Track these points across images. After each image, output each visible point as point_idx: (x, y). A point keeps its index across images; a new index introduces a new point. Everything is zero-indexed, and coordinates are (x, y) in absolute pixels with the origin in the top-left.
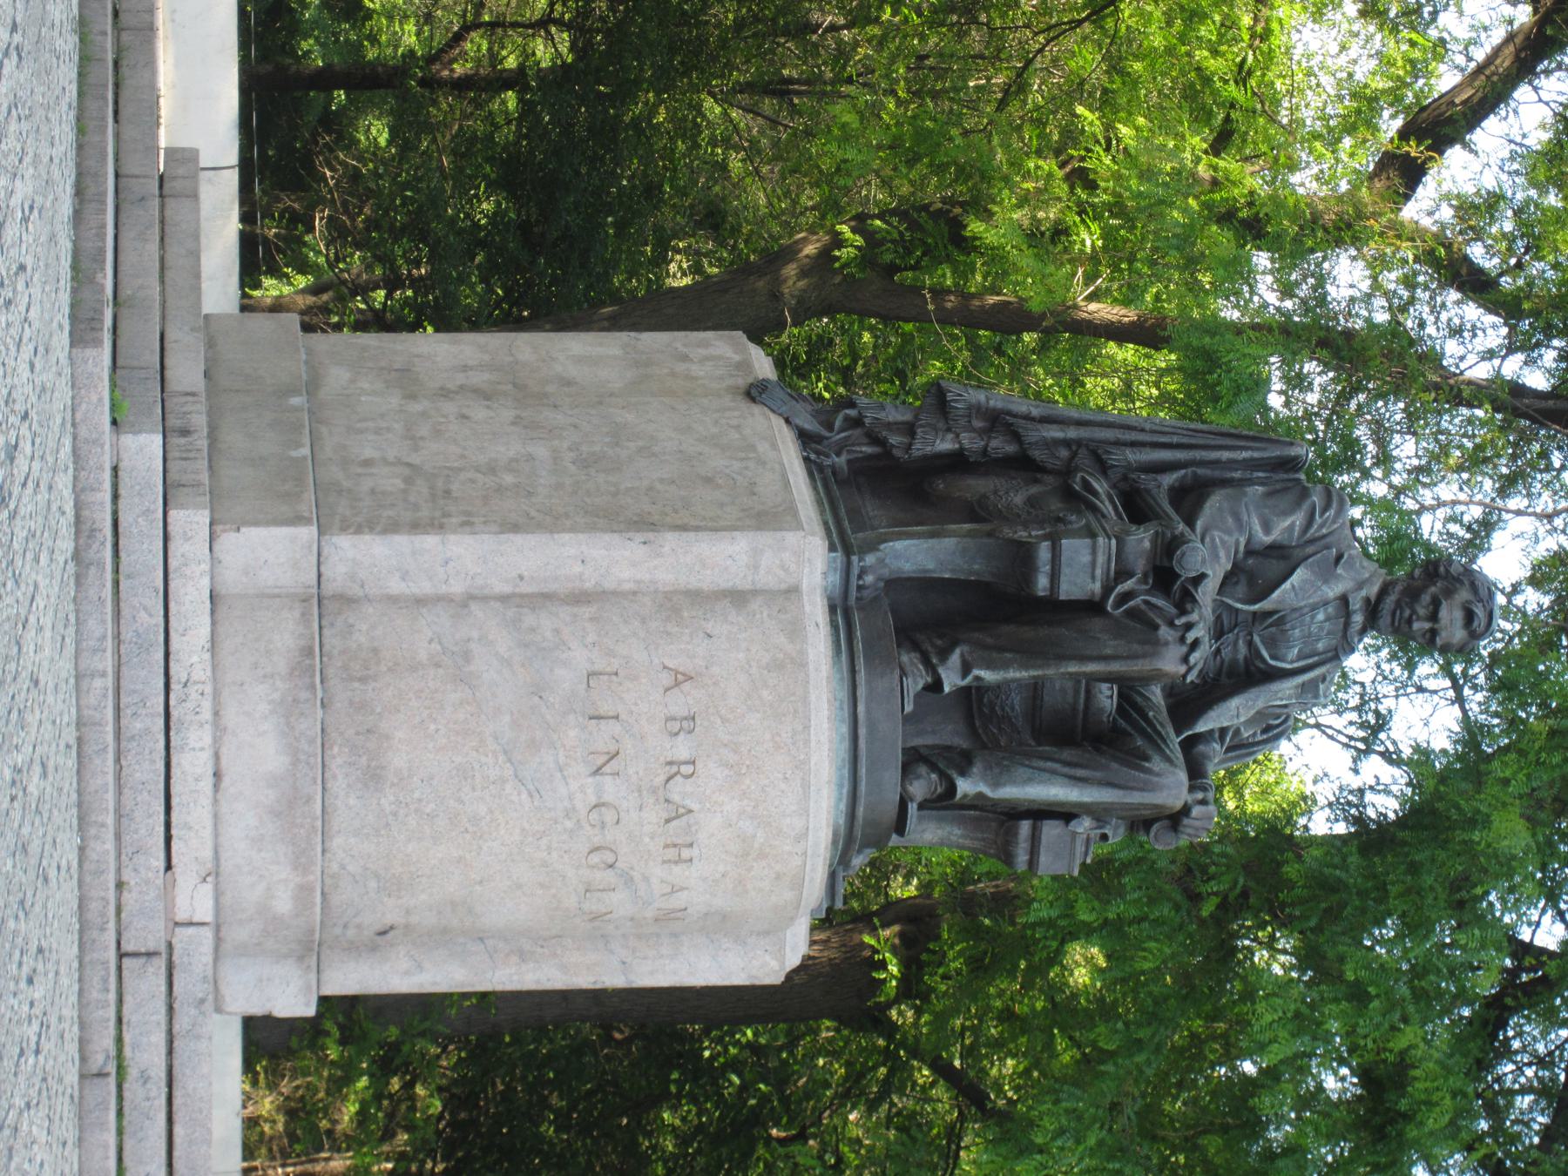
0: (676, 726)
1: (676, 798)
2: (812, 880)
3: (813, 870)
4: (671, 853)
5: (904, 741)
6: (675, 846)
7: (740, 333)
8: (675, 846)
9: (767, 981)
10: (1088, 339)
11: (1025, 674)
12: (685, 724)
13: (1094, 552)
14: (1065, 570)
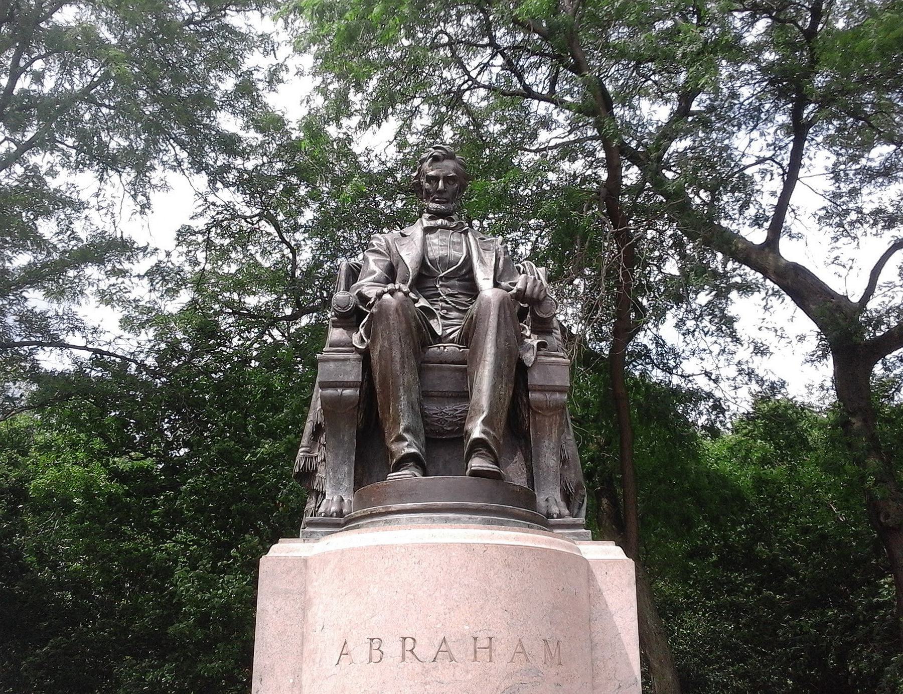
0: (376, 655)
1: (433, 653)
2: (516, 539)
3: (507, 538)
4: (483, 655)
5: (599, 561)
6: (475, 652)
7: (263, 560)
8: (475, 652)
9: (632, 572)
10: (349, 435)
11: (377, 380)
12: (375, 646)
13: (327, 360)
14: (341, 378)
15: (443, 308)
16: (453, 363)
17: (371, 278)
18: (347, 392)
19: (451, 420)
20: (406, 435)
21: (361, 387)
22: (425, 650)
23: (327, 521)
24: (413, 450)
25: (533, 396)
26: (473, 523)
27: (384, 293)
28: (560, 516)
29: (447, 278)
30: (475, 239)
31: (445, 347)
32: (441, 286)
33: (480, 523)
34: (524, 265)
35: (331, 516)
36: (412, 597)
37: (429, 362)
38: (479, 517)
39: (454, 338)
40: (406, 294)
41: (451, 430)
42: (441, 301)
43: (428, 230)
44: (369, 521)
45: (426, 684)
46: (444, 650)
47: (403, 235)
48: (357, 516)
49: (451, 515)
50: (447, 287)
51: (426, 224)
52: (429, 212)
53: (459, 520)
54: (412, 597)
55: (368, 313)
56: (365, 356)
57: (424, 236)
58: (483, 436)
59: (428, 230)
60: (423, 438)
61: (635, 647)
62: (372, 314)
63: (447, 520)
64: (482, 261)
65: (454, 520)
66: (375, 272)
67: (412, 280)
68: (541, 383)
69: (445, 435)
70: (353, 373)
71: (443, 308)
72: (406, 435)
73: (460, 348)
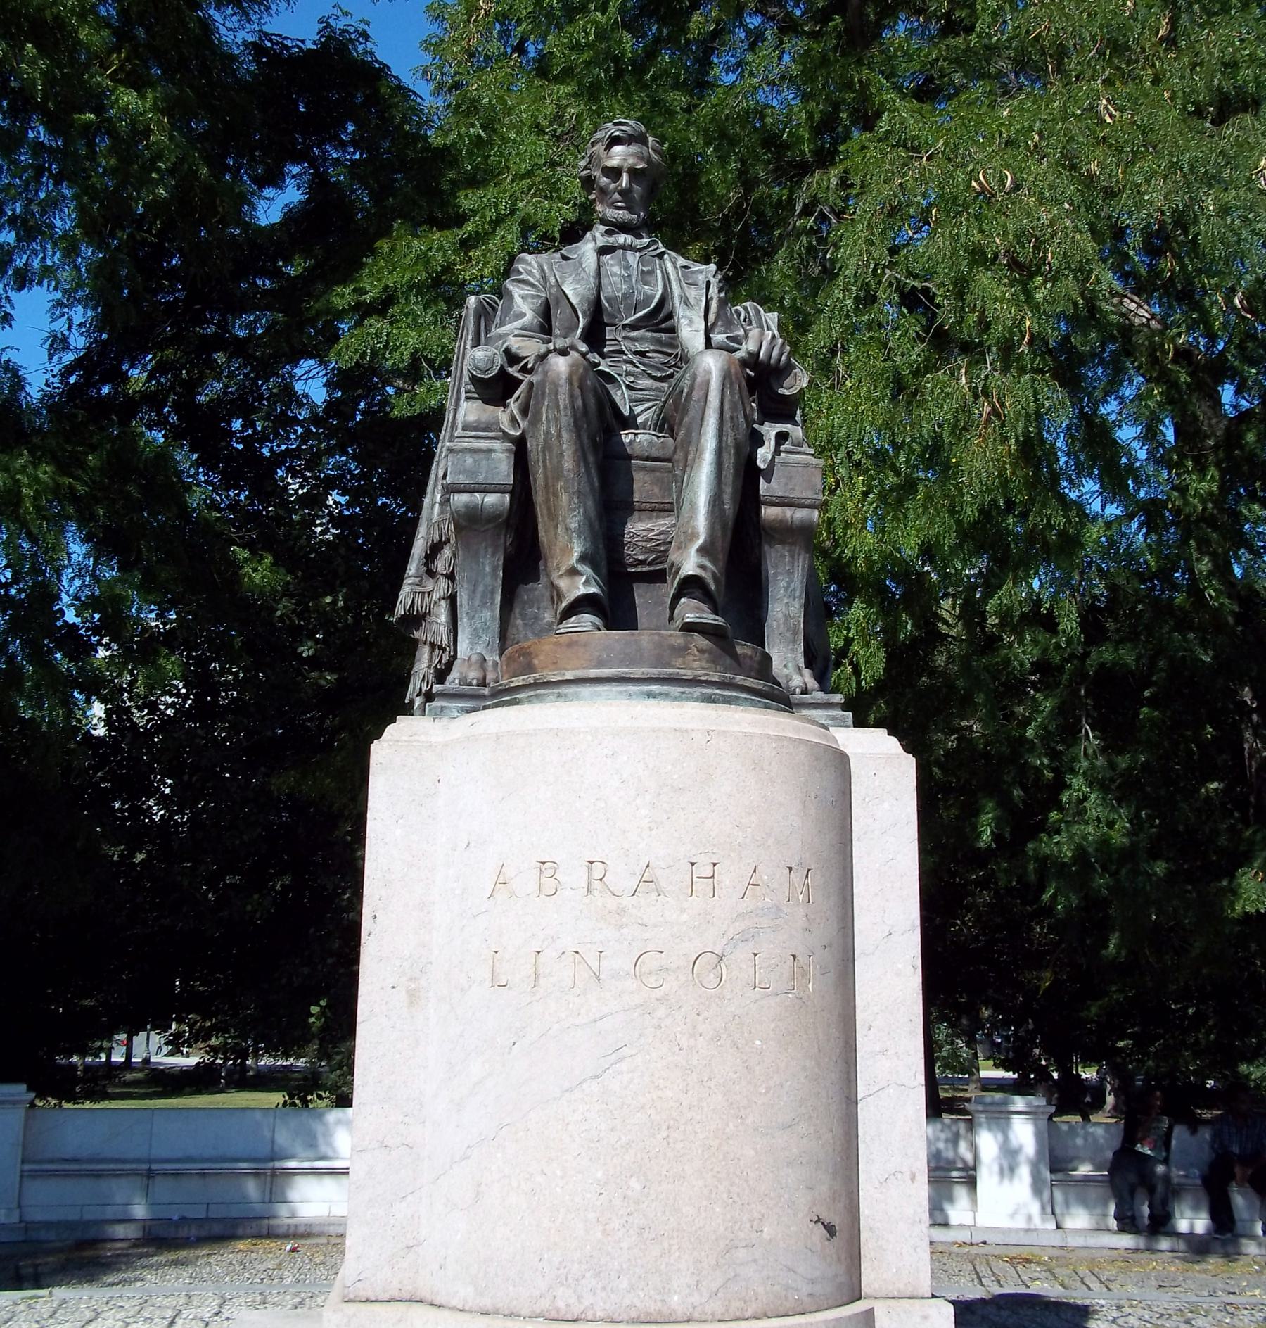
15: (628, 373)
16: (647, 459)
17: (518, 324)
18: (490, 499)
19: (644, 544)
20: (580, 567)
21: (512, 493)
22: (621, 878)
23: (464, 692)
24: (593, 589)
25: (768, 513)
26: (688, 699)
27: (549, 352)
28: (805, 691)
29: (634, 327)
30: (676, 268)
31: (636, 434)
32: (624, 338)
33: (697, 700)
34: (745, 309)
35: (470, 684)
36: (603, 805)
37: (722, 510)
38: (697, 691)
39: (647, 420)
40: (584, 355)
41: (646, 560)
42: (626, 362)
43: (603, 251)
44: (532, 693)
45: (622, 927)
46: (647, 881)
47: (565, 258)
48: (512, 685)
49: (655, 688)
50: (633, 339)
51: (602, 241)
52: (604, 222)
53: (666, 695)
54: (603, 805)
55: (520, 382)
56: (520, 449)
57: (598, 259)
58: (699, 572)
59: (603, 251)
60: (604, 571)
61: (867, 1212)
62: (531, 384)
63: (650, 695)
64: (685, 301)
65: (660, 694)
66: (523, 315)
67: (583, 329)
68: (780, 494)
69: (635, 566)
70: (502, 467)
71: (628, 373)
72: (580, 567)
73: (658, 437)
